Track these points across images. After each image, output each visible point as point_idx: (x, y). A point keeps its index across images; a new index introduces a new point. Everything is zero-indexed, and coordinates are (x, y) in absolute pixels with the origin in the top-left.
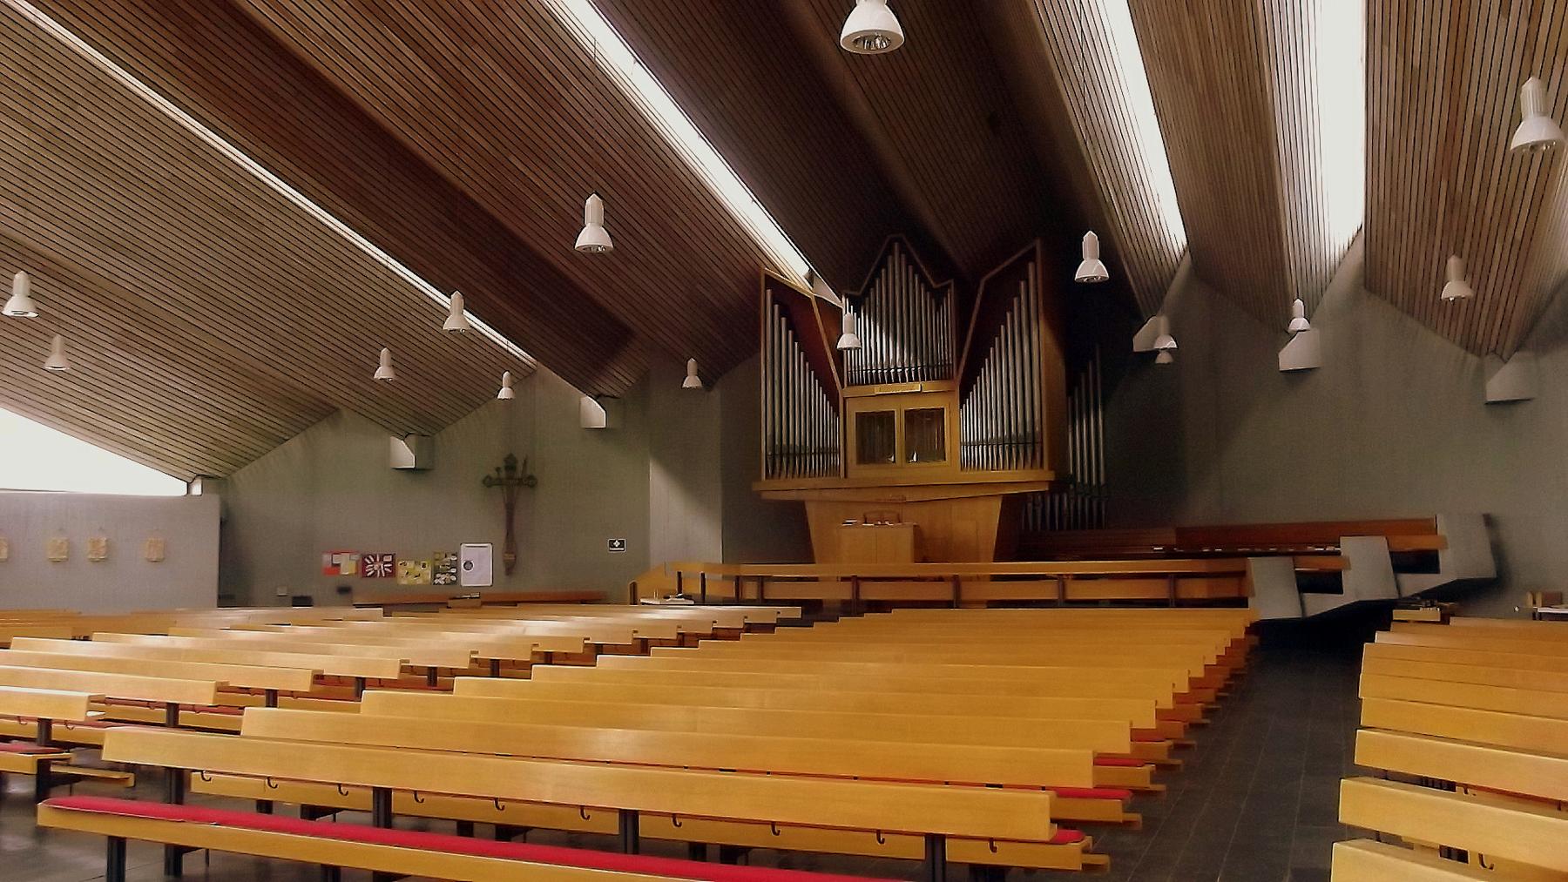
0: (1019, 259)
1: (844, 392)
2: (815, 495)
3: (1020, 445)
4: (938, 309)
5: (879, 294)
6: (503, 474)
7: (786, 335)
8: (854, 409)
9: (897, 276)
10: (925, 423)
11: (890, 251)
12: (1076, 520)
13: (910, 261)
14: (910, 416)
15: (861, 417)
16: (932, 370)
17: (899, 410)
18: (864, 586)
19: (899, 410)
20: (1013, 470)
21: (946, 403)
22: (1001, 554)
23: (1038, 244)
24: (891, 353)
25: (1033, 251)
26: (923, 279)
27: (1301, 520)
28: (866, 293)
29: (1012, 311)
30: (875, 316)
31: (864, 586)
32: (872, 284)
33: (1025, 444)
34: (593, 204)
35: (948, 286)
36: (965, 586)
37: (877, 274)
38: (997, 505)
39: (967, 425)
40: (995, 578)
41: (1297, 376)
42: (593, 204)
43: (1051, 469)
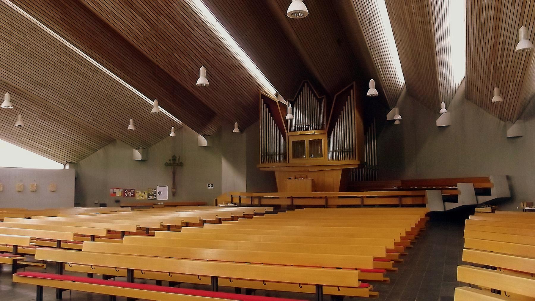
1: (288, 134)
2: (278, 169)
3: (348, 152)
4: (320, 106)
5: (300, 100)
6: (172, 162)
7: (268, 114)
8: (291, 139)
9: (306, 94)
10: (316, 144)
11: (303, 86)
12: (367, 178)
13: (310, 89)
14: (311, 142)
15: (294, 142)
16: (318, 126)
17: (307, 140)
18: (295, 200)
19: (307, 140)
20: (346, 161)
21: (323, 138)
22: (342, 189)
23: (354, 83)
24: (304, 120)
25: (353, 86)
26: (315, 95)
27: (444, 178)
28: (296, 100)
29: (345, 106)
30: (298, 108)
31: (295, 200)
32: (297, 97)
33: (350, 151)
34: (202, 70)
35: (324, 98)
36: (329, 200)
37: (299, 93)
38: (340, 172)
39: (330, 145)
40: (340, 197)
42: (202, 70)
43: (358, 160)
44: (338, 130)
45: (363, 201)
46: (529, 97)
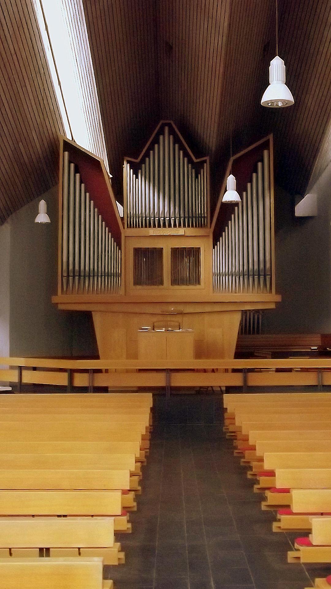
0: (160, 128)
1: (125, 232)
2: (102, 307)
3: (256, 275)
4: (197, 177)
5: (152, 162)
8: (130, 245)
9: (166, 149)
10: (187, 256)
12: (245, 330)
13: (177, 140)
14: (177, 253)
15: (138, 252)
16: (191, 220)
17: (167, 247)
18: (77, 376)
19: (167, 247)
20: (241, 294)
21: (204, 246)
22: (239, 355)
23: (271, 137)
24: (161, 206)
25: (269, 140)
26: (186, 154)
28: (143, 161)
30: (149, 178)
31: (77, 376)
32: (147, 155)
33: (259, 275)
35: (205, 161)
37: (152, 148)
38: (237, 319)
40: (278, 370)
41: (303, 220)
43: (277, 292)
44: (234, 231)
45: (71, 379)
46: (9, 220)
